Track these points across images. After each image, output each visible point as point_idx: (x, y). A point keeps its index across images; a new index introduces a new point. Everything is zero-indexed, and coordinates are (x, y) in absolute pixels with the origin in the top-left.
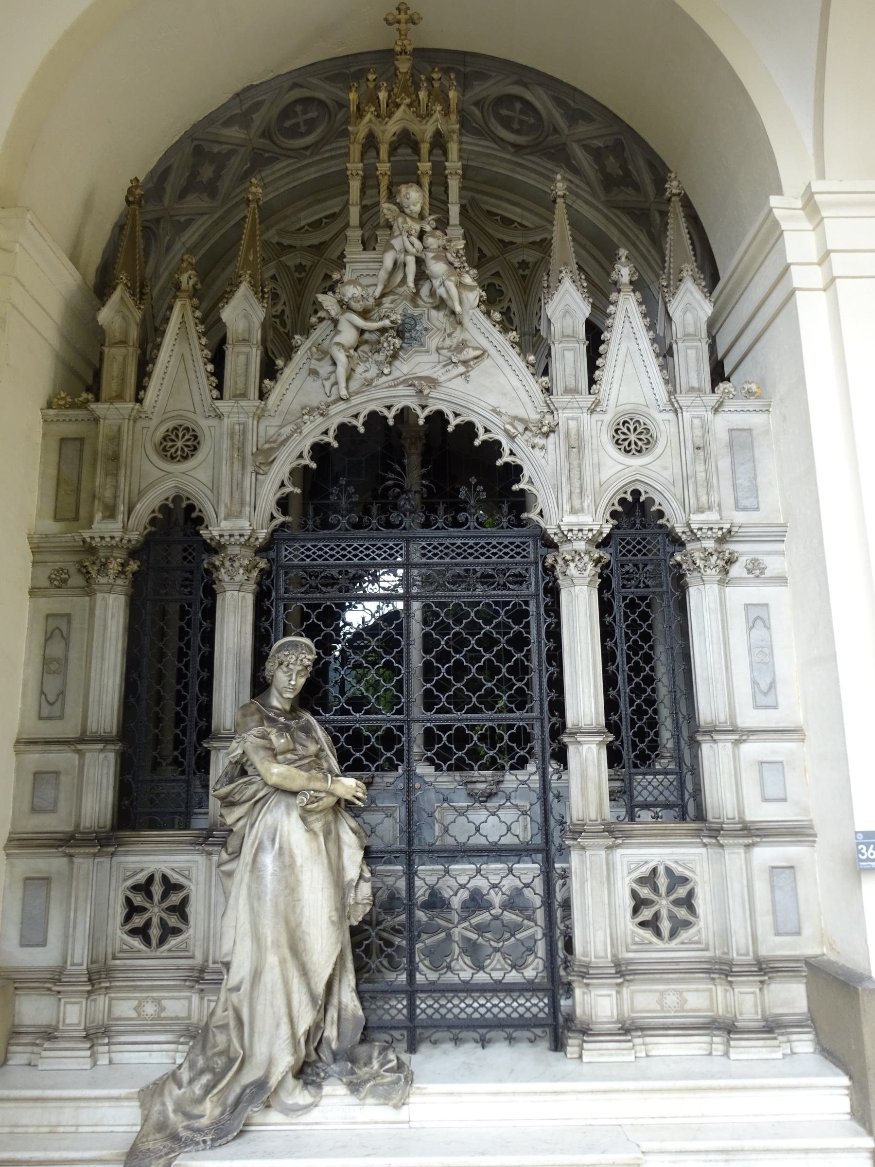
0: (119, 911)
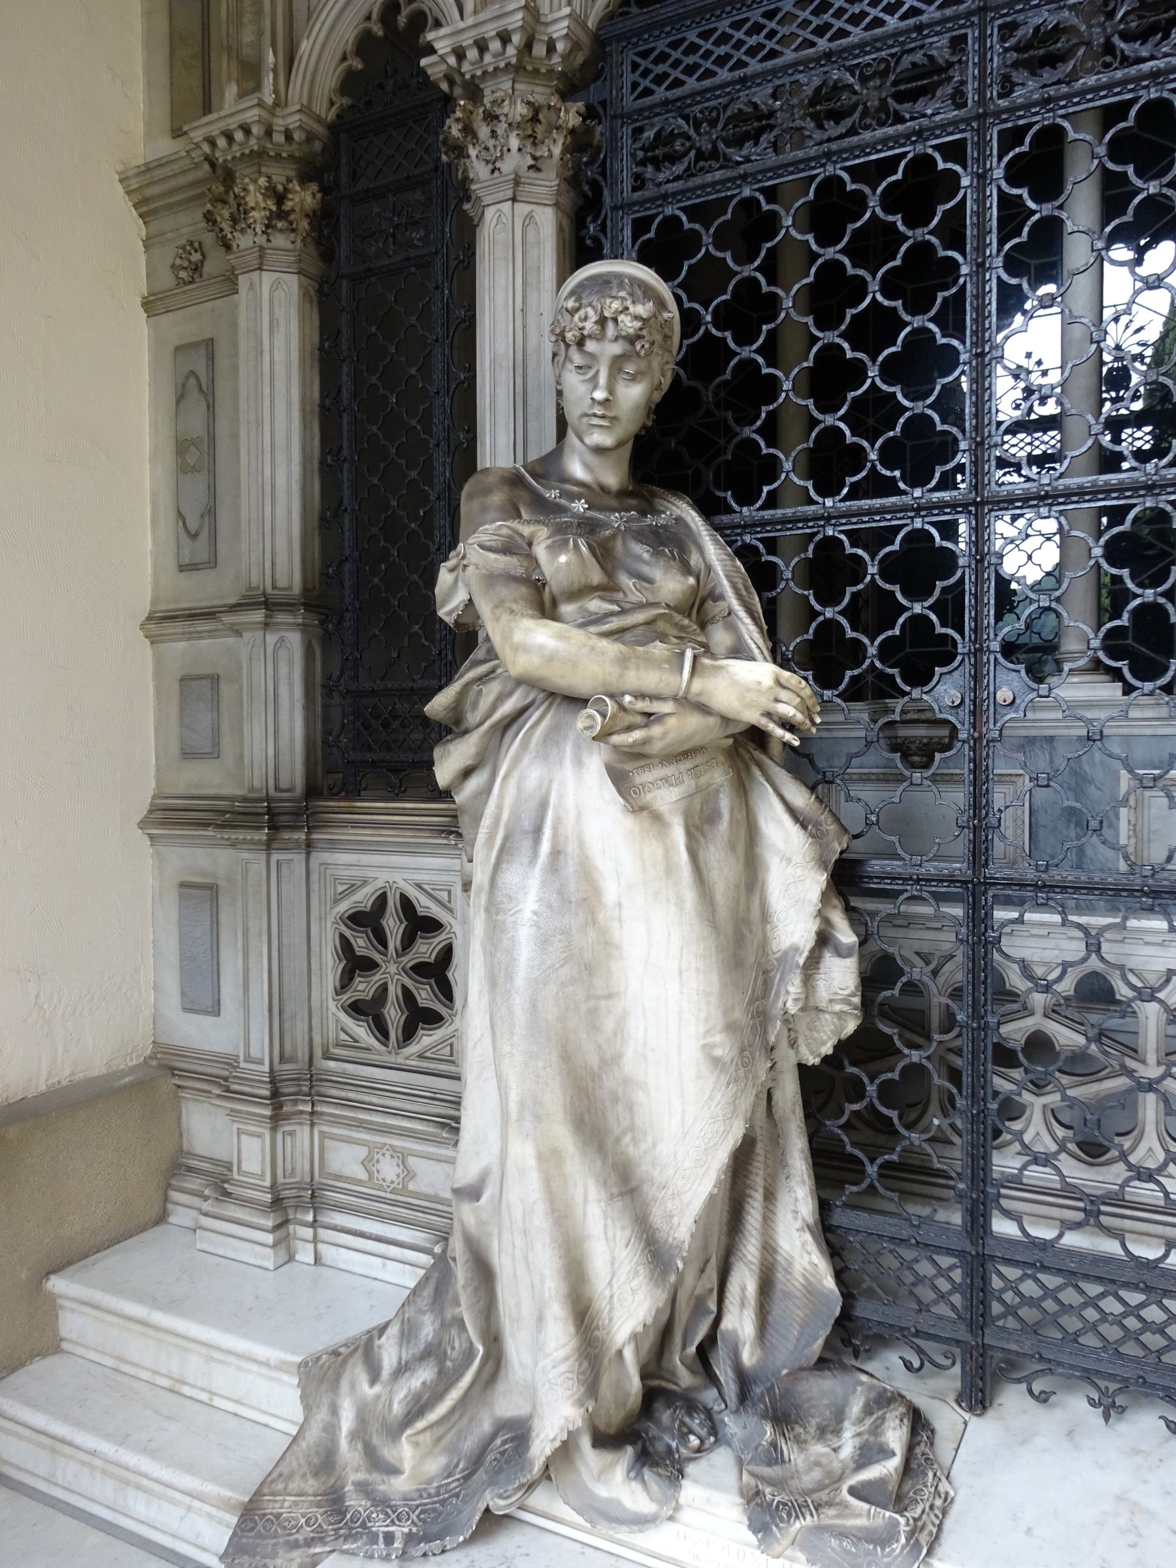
0: (330, 967)
